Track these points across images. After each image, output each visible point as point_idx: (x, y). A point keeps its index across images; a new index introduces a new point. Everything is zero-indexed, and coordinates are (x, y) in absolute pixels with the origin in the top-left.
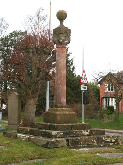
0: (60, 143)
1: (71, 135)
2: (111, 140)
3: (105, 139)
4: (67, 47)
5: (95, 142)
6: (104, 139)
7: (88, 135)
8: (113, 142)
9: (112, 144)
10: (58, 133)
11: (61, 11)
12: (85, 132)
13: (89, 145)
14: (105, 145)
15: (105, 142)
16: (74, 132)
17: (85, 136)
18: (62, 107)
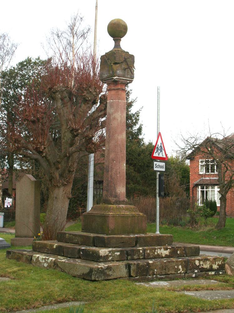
0: (115, 272)
1: (135, 257)
2: (211, 266)
3: (199, 263)
5: (181, 270)
8: (215, 270)
9: (213, 273)
10: (110, 252)
12: (162, 250)
13: (170, 276)
14: (199, 275)
16: (142, 250)
17: (162, 257)
18: (118, 203)
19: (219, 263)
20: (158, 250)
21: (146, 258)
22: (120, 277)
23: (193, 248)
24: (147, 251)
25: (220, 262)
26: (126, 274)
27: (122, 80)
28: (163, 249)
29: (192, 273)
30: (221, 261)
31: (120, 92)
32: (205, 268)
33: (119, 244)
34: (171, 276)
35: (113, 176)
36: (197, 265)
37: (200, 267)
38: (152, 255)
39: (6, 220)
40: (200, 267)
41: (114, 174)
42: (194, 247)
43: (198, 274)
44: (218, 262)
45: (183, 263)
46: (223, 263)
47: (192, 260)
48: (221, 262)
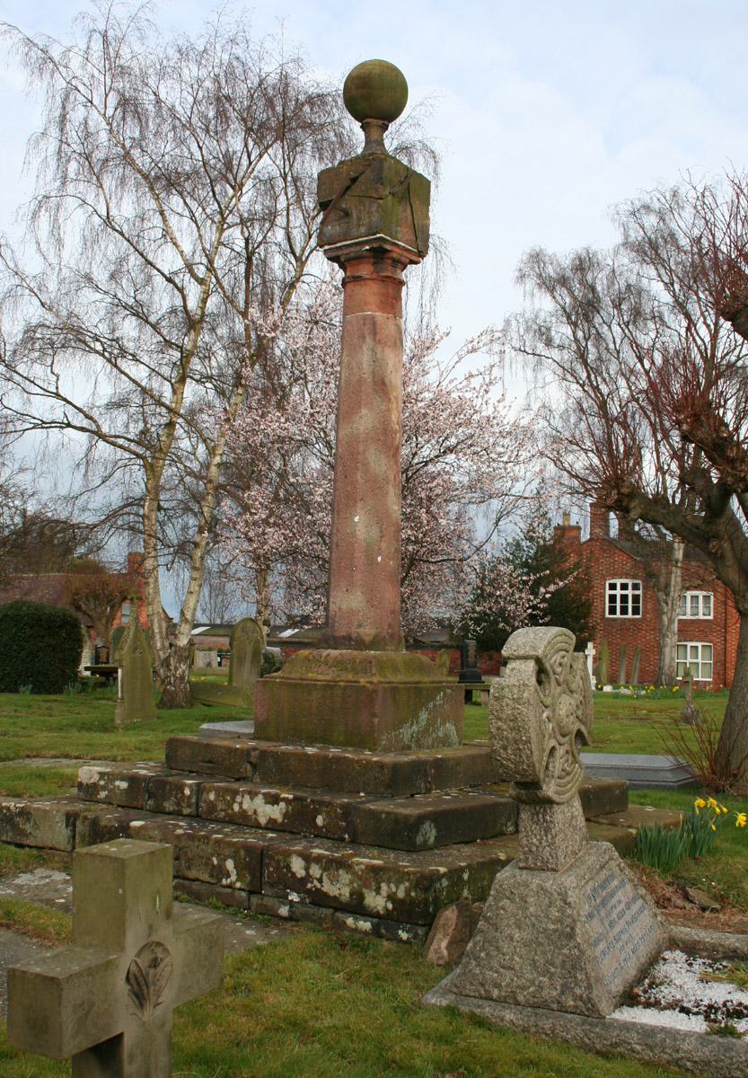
0: (38, 828)
1: (169, 806)
2: (358, 897)
3: (307, 869)
4: (403, 275)
5: (233, 878)
6: (297, 866)
7: (272, 825)
8: (377, 915)
9: (365, 925)
10: (102, 775)
11: (377, 71)
12: (259, 800)
13: (195, 886)
14: (306, 917)
15: (309, 892)
16: (190, 786)
17: (258, 826)
18: (331, 643)
19: (394, 889)
20: (243, 796)
22: (50, 845)
23: (383, 816)
24: (208, 793)
25: (402, 887)
26: (66, 841)
27: (345, 251)
28: (260, 797)
29: (276, 900)
30: (407, 884)
32: (332, 894)
33: (201, 764)
34: (197, 888)
36: (299, 876)
37: (309, 886)
38: (222, 810)
40: (309, 886)
42: (388, 813)
43: (300, 910)
44: (392, 885)
45: (242, 853)
46: (413, 894)
47: (278, 853)
48: (407, 891)
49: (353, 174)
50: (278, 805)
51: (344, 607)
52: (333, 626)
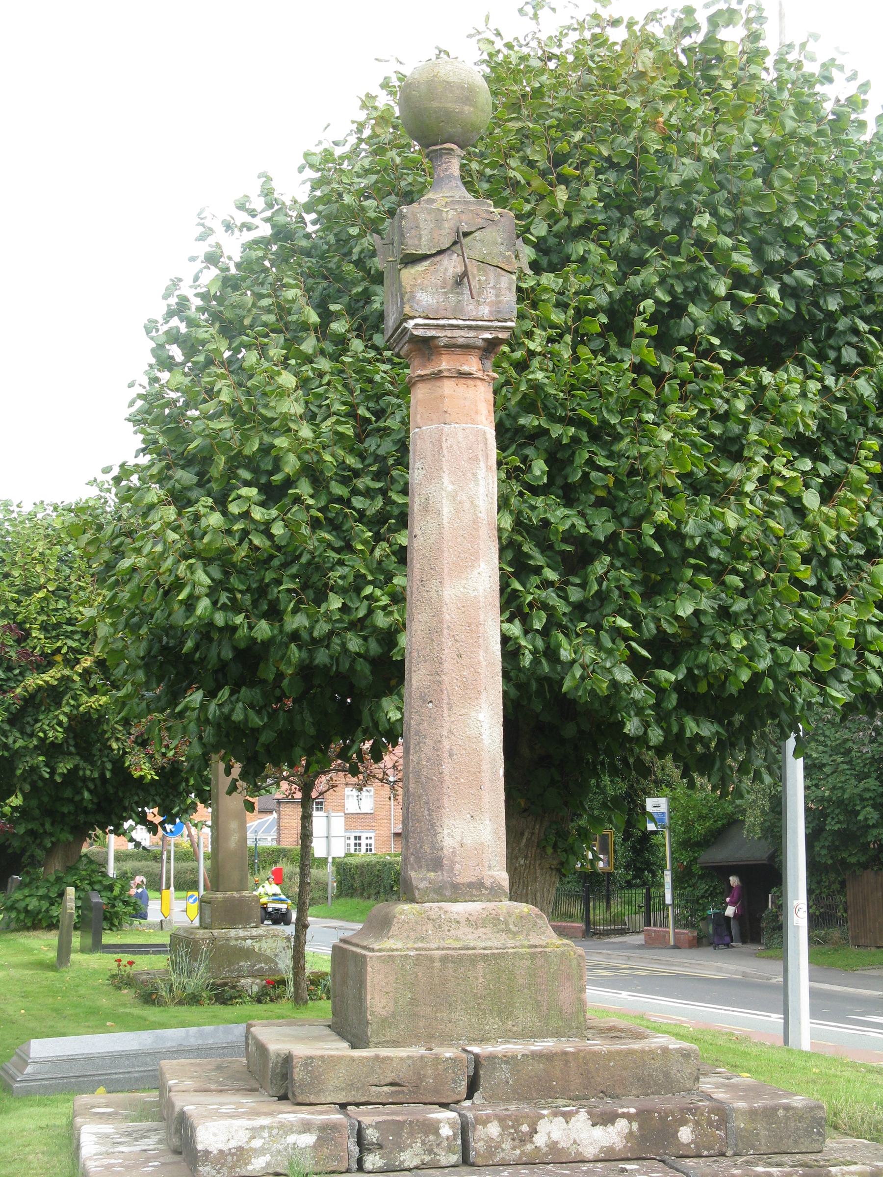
10: (255, 1132)
18: (448, 893)
21: (479, 1161)
27: (449, 333)
31: (448, 387)
35: (425, 772)
39: (819, 883)
41: (429, 759)
49: (465, 228)
50: (613, 1124)
51: (468, 841)
52: (452, 869)
